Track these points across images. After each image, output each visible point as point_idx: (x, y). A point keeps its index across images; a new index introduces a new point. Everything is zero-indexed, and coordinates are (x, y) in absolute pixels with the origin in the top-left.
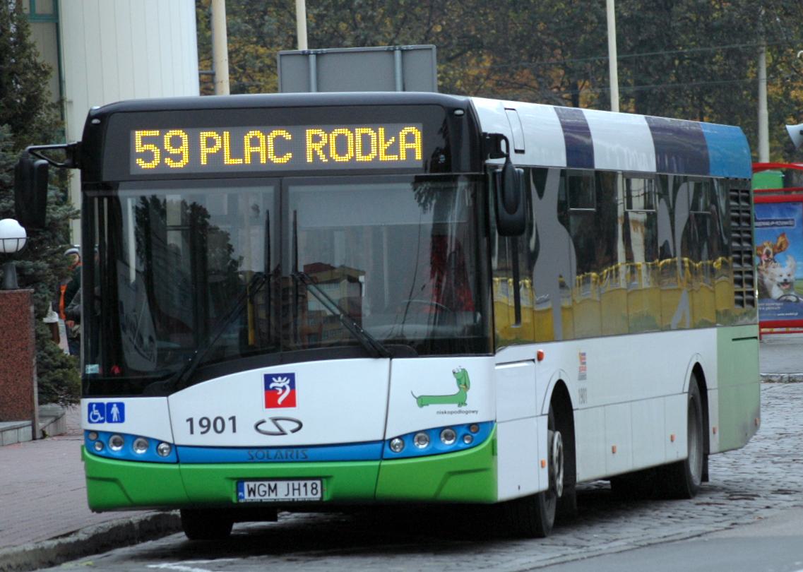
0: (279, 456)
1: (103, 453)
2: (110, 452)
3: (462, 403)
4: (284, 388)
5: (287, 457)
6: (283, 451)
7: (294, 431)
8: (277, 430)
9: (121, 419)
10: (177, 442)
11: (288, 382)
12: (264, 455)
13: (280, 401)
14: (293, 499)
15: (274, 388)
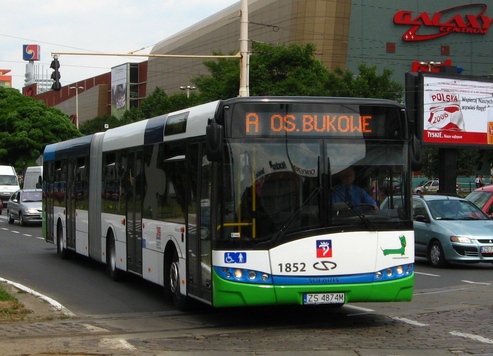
0: (325, 281)
1: (231, 278)
2: (235, 278)
3: (403, 253)
4: (326, 248)
5: (328, 282)
6: (327, 279)
7: (332, 268)
8: (324, 268)
9: (244, 261)
10: (274, 273)
11: (328, 244)
12: (317, 280)
13: (324, 254)
14: (331, 302)
15: (321, 247)
